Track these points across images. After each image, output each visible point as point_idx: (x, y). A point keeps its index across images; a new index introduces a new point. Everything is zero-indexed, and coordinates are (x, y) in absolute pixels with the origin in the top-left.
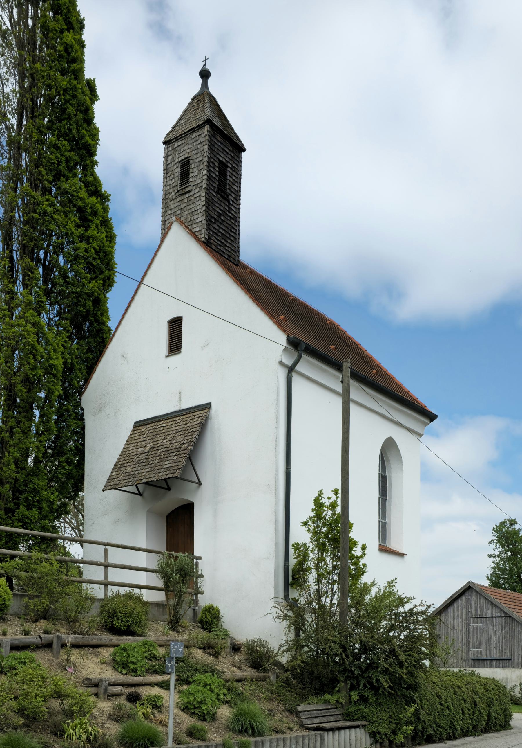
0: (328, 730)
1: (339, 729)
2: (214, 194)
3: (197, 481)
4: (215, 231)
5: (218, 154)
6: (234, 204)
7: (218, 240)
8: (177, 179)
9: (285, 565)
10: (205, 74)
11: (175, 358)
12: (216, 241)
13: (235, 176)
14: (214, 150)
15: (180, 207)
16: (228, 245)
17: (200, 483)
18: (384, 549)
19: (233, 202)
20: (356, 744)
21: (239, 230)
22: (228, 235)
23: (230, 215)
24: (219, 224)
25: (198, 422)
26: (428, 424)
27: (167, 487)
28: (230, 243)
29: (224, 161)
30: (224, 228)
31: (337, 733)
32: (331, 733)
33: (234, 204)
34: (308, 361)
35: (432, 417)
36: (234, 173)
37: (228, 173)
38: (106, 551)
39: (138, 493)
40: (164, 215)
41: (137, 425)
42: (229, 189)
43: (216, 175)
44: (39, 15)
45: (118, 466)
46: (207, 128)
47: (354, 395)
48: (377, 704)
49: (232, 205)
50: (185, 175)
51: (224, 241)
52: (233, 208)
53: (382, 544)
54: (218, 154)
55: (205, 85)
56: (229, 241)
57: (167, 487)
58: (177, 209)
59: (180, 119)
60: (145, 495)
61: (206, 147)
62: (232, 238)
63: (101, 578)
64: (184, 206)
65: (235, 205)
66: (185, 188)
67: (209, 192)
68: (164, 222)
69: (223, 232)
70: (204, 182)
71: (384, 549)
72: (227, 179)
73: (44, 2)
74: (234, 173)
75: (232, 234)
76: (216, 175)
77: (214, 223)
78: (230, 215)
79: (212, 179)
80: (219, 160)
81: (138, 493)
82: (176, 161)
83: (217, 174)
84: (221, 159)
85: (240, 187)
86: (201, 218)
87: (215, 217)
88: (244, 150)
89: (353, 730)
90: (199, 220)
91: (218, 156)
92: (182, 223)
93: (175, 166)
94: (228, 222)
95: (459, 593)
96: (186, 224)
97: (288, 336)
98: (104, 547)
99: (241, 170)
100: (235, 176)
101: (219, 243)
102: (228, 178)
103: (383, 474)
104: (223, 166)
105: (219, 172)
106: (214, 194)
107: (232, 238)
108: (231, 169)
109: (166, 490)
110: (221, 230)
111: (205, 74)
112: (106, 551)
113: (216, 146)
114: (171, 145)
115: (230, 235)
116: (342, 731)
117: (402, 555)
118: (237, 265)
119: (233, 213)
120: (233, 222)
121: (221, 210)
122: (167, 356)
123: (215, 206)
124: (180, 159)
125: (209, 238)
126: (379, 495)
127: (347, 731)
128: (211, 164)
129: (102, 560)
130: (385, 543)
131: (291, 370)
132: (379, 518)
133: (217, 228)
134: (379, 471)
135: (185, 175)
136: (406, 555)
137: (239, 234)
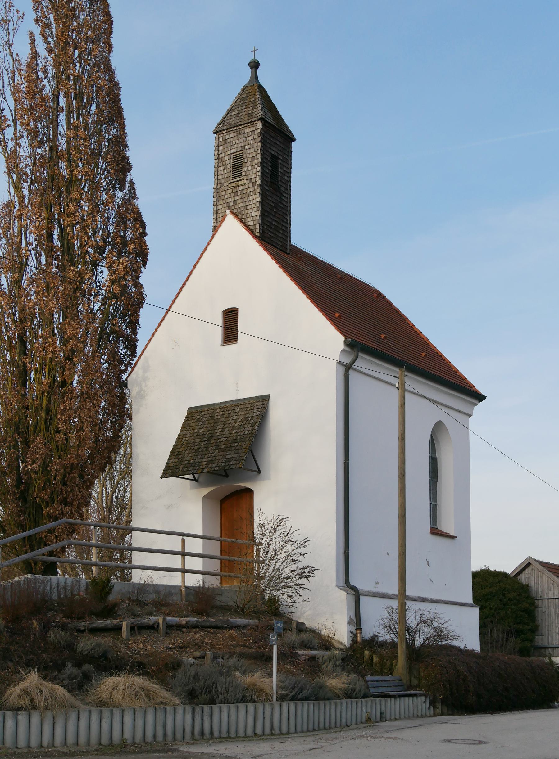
0: (390, 697)
1: (400, 696)
2: (267, 188)
3: (257, 470)
4: (268, 224)
5: (271, 149)
6: (285, 195)
7: (272, 232)
8: (229, 170)
9: (345, 552)
10: (255, 65)
11: (231, 348)
12: (270, 234)
13: (285, 167)
14: (266, 146)
15: (233, 199)
16: (280, 235)
17: (259, 472)
18: (436, 531)
19: (284, 192)
20: (413, 710)
21: (290, 219)
22: (280, 226)
23: (282, 206)
24: (272, 217)
25: (258, 413)
26: (477, 405)
28: (282, 234)
29: (276, 154)
30: (277, 220)
31: (398, 700)
32: (393, 699)
33: (285, 195)
34: (363, 358)
35: (480, 398)
36: (285, 164)
37: (279, 166)
38: (183, 541)
39: (193, 478)
40: (216, 204)
41: (191, 411)
42: (281, 181)
43: (269, 169)
45: (174, 453)
46: (259, 124)
49: (283, 195)
50: (237, 168)
51: (276, 233)
52: (284, 198)
53: (433, 527)
54: (271, 149)
55: (255, 76)
56: (281, 231)
58: (229, 200)
59: (230, 110)
60: (200, 480)
61: (259, 144)
62: (283, 228)
63: (179, 566)
64: (236, 198)
65: (286, 195)
66: (238, 181)
67: (263, 187)
68: (217, 212)
69: (276, 224)
70: (258, 178)
71: (436, 531)
72: (278, 171)
73: (101, 1)
74: (285, 164)
75: (284, 224)
76: (269, 169)
77: (268, 216)
78: (282, 206)
79: (265, 174)
80: (271, 154)
81: (193, 478)
82: (229, 152)
83: (270, 168)
84: (273, 153)
85: (290, 177)
86: (256, 214)
87: (268, 210)
88: (294, 140)
89: (411, 698)
90: (253, 214)
91: (270, 151)
92: (236, 216)
93: (227, 158)
94: (280, 213)
95: (525, 564)
96: (240, 217)
97: (346, 339)
98: (181, 537)
99: (291, 160)
100: (285, 167)
101: (272, 235)
102: (280, 170)
103: (433, 456)
104: (274, 158)
106: (267, 188)
107: (283, 228)
108: (282, 160)
110: (274, 223)
111: (255, 65)
112: (183, 541)
113: (268, 141)
114: (222, 135)
115: (282, 225)
116: (402, 699)
117: (453, 537)
119: (284, 203)
120: (284, 212)
121: (273, 202)
123: (268, 199)
124: (232, 151)
125: (263, 232)
126: (430, 477)
127: (406, 698)
128: (265, 165)
129: (179, 549)
130: (436, 526)
131: (348, 368)
132: (430, 501)
133: (271, 221)
134: (430, 453)
135: (237, 168)
137: (290, 223)
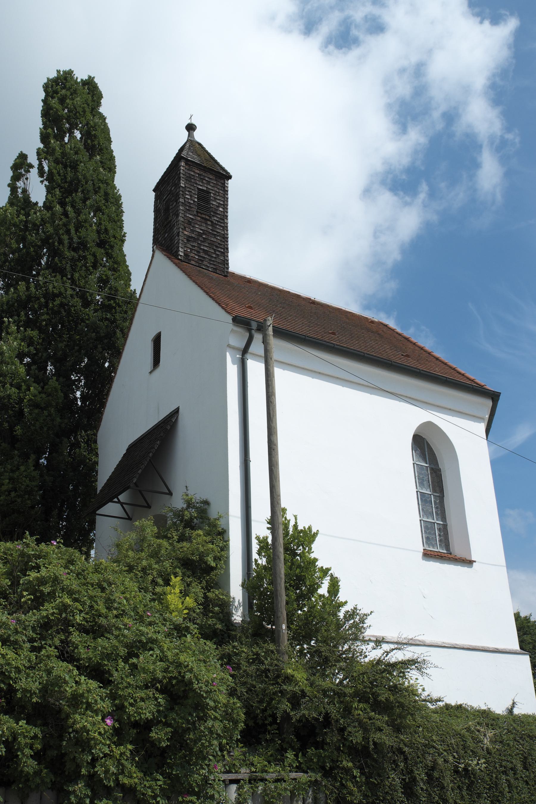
10: (191, 128)
17: (170, 494)
27: (146, 505)
39: (126, 517)
44: (55, 129)
47: (276, 355)
48: (263, 770)
57: (146, 505)
80: (198, 188)
83: (196, 200)
84: (199, 187)
88: (229, 177)
103: (433, 467)
105: (198, 198)
109: (146, 509)
111: (191, 128)
118: (226, 276)
121: (201, 229)
122: (151, 373)
136: (475, 562)
